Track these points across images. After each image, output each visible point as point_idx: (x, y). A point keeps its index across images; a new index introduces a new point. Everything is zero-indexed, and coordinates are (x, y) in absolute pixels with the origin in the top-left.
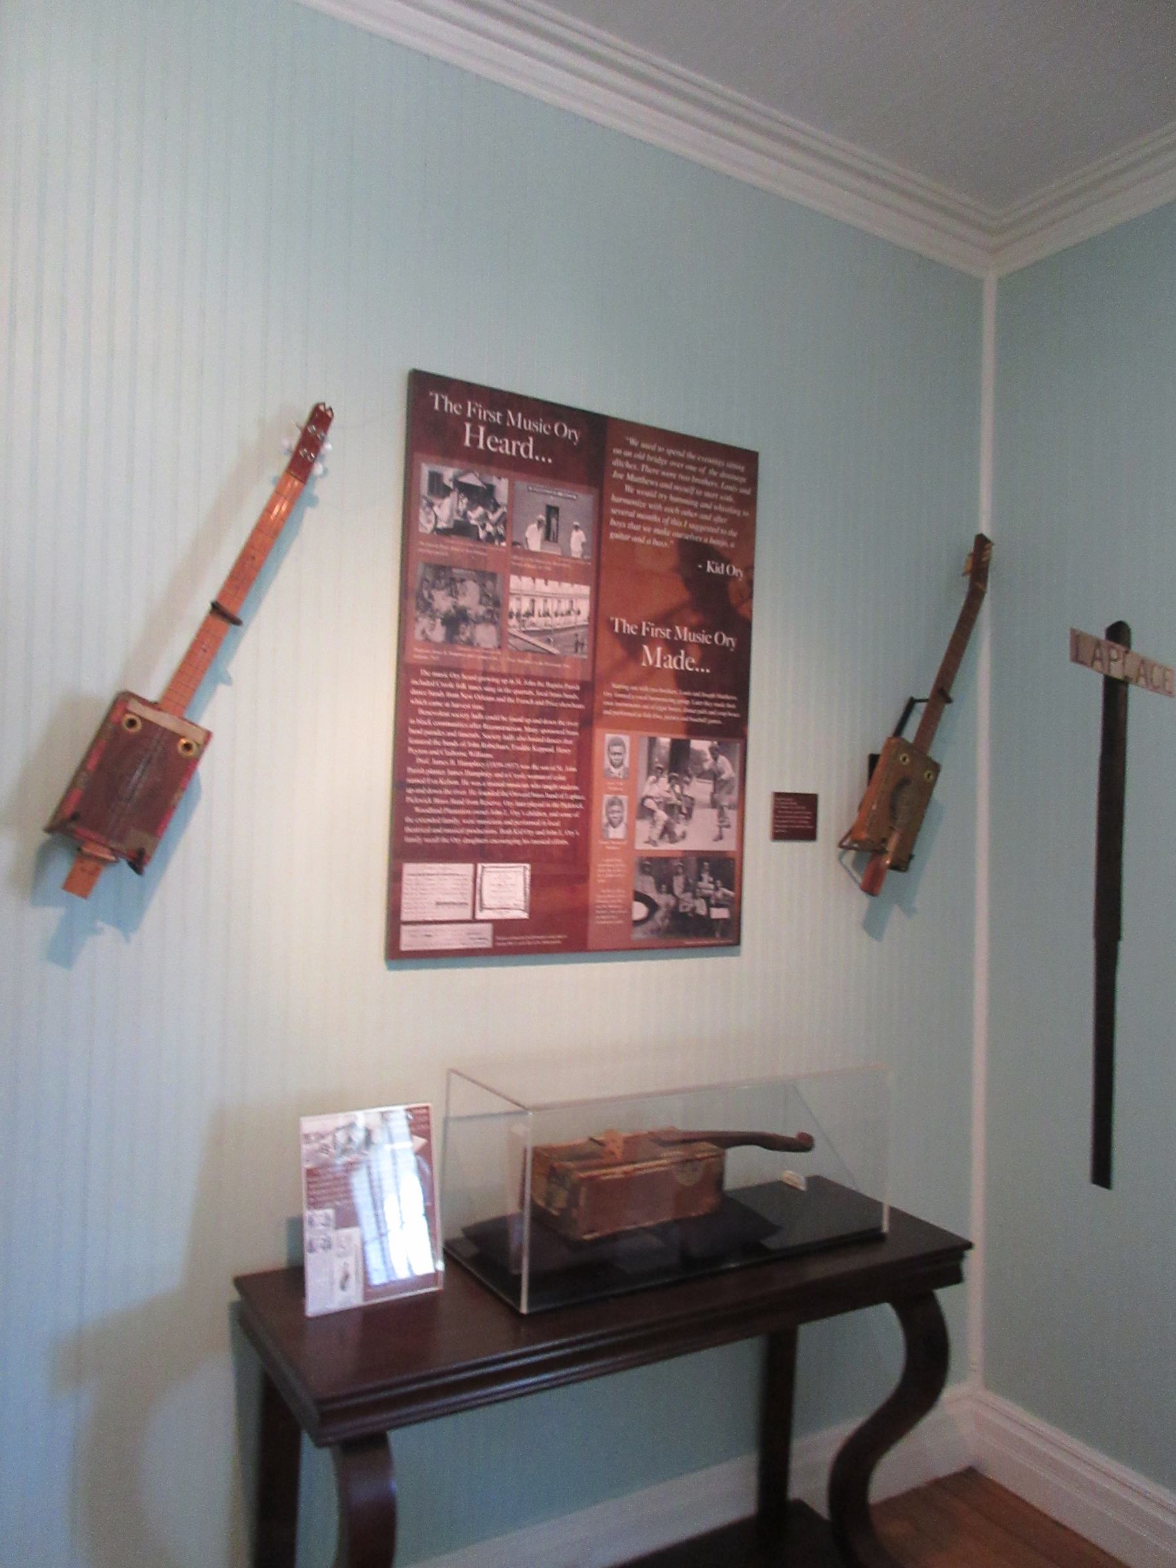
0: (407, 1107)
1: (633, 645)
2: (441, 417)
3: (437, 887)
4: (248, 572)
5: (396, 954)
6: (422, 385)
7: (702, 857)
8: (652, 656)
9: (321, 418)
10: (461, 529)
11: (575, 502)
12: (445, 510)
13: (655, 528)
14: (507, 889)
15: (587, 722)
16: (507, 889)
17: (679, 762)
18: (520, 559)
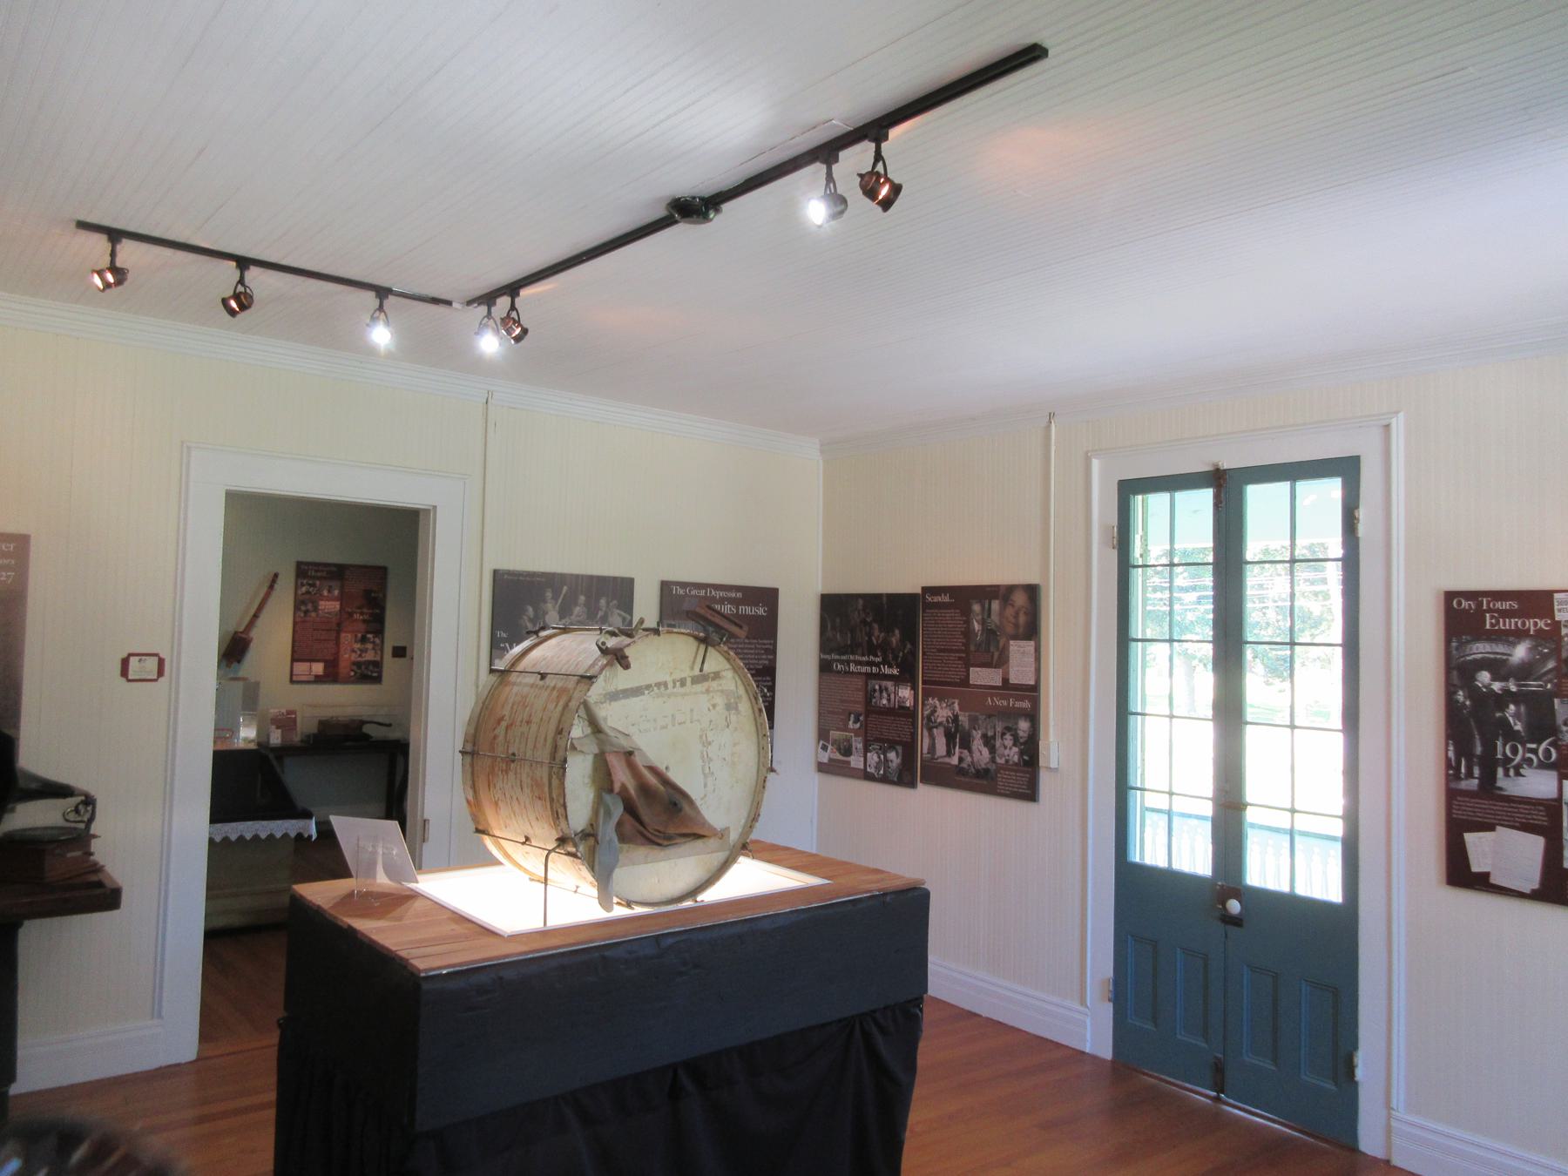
1: (351, 615)
2: (304, 571)
3: (301, 668)
5: (292, 681)
6: (299, 564)
8: (356, 616)
9: (276, 575)
10: (308, 592)
11: (335, 584)
14: (318, 668)
15: (338, 633)
16: (318, 668)
17: (364, 640)
18: (322, 598)
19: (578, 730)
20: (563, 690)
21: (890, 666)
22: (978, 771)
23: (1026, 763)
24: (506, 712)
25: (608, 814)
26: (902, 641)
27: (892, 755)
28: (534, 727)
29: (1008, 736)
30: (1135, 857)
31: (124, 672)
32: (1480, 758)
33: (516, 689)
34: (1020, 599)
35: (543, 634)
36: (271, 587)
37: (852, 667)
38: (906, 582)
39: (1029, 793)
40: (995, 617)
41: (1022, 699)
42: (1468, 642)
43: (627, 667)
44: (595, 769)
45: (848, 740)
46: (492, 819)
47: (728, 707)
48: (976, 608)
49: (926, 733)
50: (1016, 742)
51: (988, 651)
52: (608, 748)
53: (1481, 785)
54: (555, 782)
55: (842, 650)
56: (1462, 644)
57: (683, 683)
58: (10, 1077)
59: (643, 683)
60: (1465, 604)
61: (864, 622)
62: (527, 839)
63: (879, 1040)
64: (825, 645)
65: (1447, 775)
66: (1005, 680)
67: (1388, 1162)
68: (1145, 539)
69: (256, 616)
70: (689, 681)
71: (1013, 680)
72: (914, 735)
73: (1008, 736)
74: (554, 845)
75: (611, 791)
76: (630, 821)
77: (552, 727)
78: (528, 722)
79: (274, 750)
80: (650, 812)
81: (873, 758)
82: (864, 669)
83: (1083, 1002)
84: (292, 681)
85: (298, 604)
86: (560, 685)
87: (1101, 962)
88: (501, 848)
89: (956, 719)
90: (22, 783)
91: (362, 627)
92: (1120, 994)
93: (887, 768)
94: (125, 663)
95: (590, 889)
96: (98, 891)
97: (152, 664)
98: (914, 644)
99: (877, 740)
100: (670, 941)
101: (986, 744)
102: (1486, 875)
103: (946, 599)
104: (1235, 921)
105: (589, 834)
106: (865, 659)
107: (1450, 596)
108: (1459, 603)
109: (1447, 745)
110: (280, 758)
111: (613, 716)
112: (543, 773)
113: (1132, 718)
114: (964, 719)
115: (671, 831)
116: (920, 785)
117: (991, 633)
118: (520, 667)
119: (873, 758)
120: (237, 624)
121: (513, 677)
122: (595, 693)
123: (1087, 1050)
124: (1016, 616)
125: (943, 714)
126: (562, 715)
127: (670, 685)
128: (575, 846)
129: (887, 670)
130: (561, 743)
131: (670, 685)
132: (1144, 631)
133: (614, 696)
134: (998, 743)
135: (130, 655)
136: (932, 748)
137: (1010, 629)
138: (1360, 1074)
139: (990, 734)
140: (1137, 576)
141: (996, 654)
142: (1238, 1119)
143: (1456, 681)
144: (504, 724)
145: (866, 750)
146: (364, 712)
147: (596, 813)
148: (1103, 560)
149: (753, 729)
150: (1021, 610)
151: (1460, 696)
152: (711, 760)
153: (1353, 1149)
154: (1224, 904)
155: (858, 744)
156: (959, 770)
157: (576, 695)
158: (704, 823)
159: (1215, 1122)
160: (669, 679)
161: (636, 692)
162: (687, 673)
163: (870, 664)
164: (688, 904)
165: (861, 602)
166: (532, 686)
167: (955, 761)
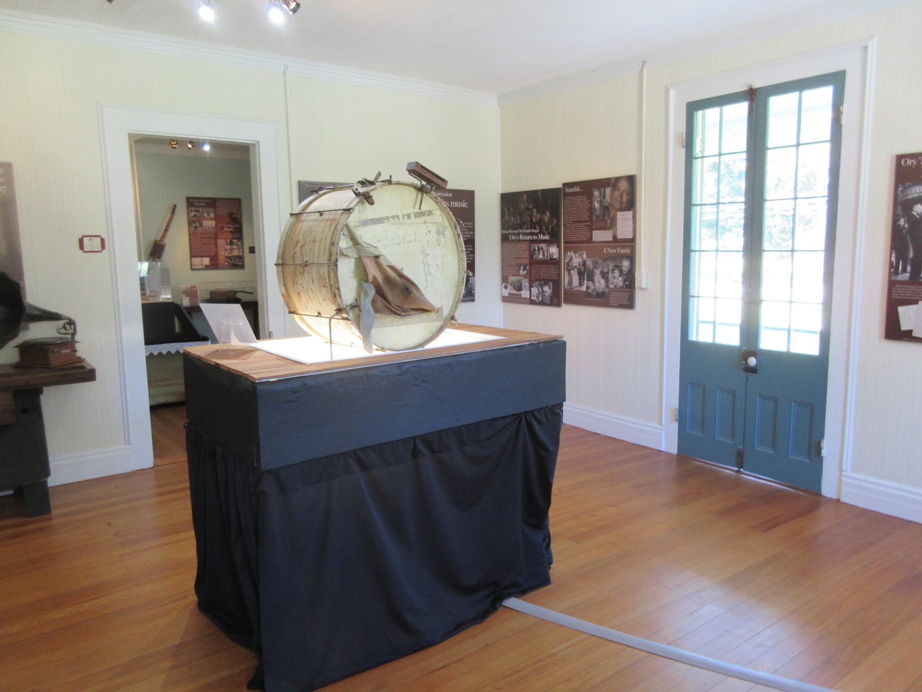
0: (197, 349)
1: (222, 228)
2: (191, 202)
3: (197, 261)
4: (168, 226)
5: (192, 269)
6: (188, 199)
7: (236, 257)
8: (225, 229)
9: (175, 206)
11: (211, 210)
12: (193, 214)
13: (224, 211)
14: (207, 261)
15: (216, 239)
16: (207, 261)
17: (231, 243)
19: (344, 243)
20: (334, 220)
21: (544, 234)
22: (598, 294)
23: (627, 286)
24: (300, 237)
25: (366, 294)
26: (551, 218)
27: (546, 288)
28: (317, 244)
29: (616, 271)
30: (693, 337)
31: (81, 246)
32: (912, 260)
33: (305, 223)
34: (623, 185)
35: (321, 192)
36: (173, 213)
37: (521, 237)
38: (554, 182)
39: (629, 304)
40: (608, 199)
41: (624, 247)
42: (910, 186)
43: (372, 203)
44: (357, 268)
45: (520, 282)
46: (298, 304)
47: (438, 233)
48: (596, 193)
49: (566, 273)
50: (621, 274)
51: (603, 220)
52: (363, 255)
53: (911, 278)
54: (332, 274)
55: (515, 227)
56: (905, 188)
57: (409, 216)
58: (46, 472)
59: (384, 216)
60: (909, 162)
61: (527, 209)
62: (319, 313)
63: (537, 428)
64: (505, 225)
65: (890, 272)
66: (615, 237)
67: (838, 500)
68: (703, 142)
69: (166, 231)
70: (412, 216)
71: (619, 236)
72: (559, 275)
73: (616, 271)
74: (335, 313)
75: (367, 281)
76: (380, 300)
77: (328, 243)
78: (314, 242)
79: (186, 308)
80: (393, 294)
81: (535, 291)
82: (528, 238)
83: (660, 423)
84: (192, 269)
85: (191, 222)
86: (331, 217)
87: (671, 399)
88: (304, 322)
89: (584, 263)
90: (28, 311)
91: (230, 235)
92: (682, 418)
93: (543, 296)
94: (81, 241)
95: (359, 342)
96: (81, 371)
97: (97, 242)
98: (559, 220)
99: (537, 280)
100: (408, 366)
101: (603, 277)
102: (910, 332)
103: (577, 189)
104: (753, 370)
105: (355, 306)
106: (529, 231)
107: (900, 158)
108: (906, 162)
109: (891, 254)
110: (190, 313)
111: (366, 235)
112: (324, 271)
113: (691, 299)
114: (589, 263)
115: (406, 306)
116: (563, 305)
117: (605, 209)
118: (308, 210)
119: (535, 291)
120: (155, 235)
121: (304, 217)
122: (353, 220)
123: (663, 449)
124: (621, 197)
125: (577, 261)
126: (333, 234)
127: (401, 218)
128: (347, 313)
129: (542, 237)
130: (334, 250)
131: (401, 218)
132: (701, 199)
133: (366, 223)
134: (610, 276)
135: (83, 236)
136: (570, 283)
137: (617, 205)
138: (824, 452)
139: (605, 270)
140: (697, 164)
141: (609, 221)
142: (750, 481)
143: (899, 211)
144: (299, 245)
145: (531, 287)
146: (236, 287)
147: (359, 294)
148: (677, 155)
149: (455, 247)
150: (623, 192)
151: (902, 222)
152: (429, 265)
153: (819, 494)
154: (746, 361)
155: (526, 283)
156: (587, 294)
157: (342, 220)
158: (426, 302)
159: (738, 483)
160: (400, 214)
161: (379, 221)
162: (411, 211)
163: (532, 234)
164: (420, 349)
165: (525, 196)
166: (315, 220)
167: (584, 289)
